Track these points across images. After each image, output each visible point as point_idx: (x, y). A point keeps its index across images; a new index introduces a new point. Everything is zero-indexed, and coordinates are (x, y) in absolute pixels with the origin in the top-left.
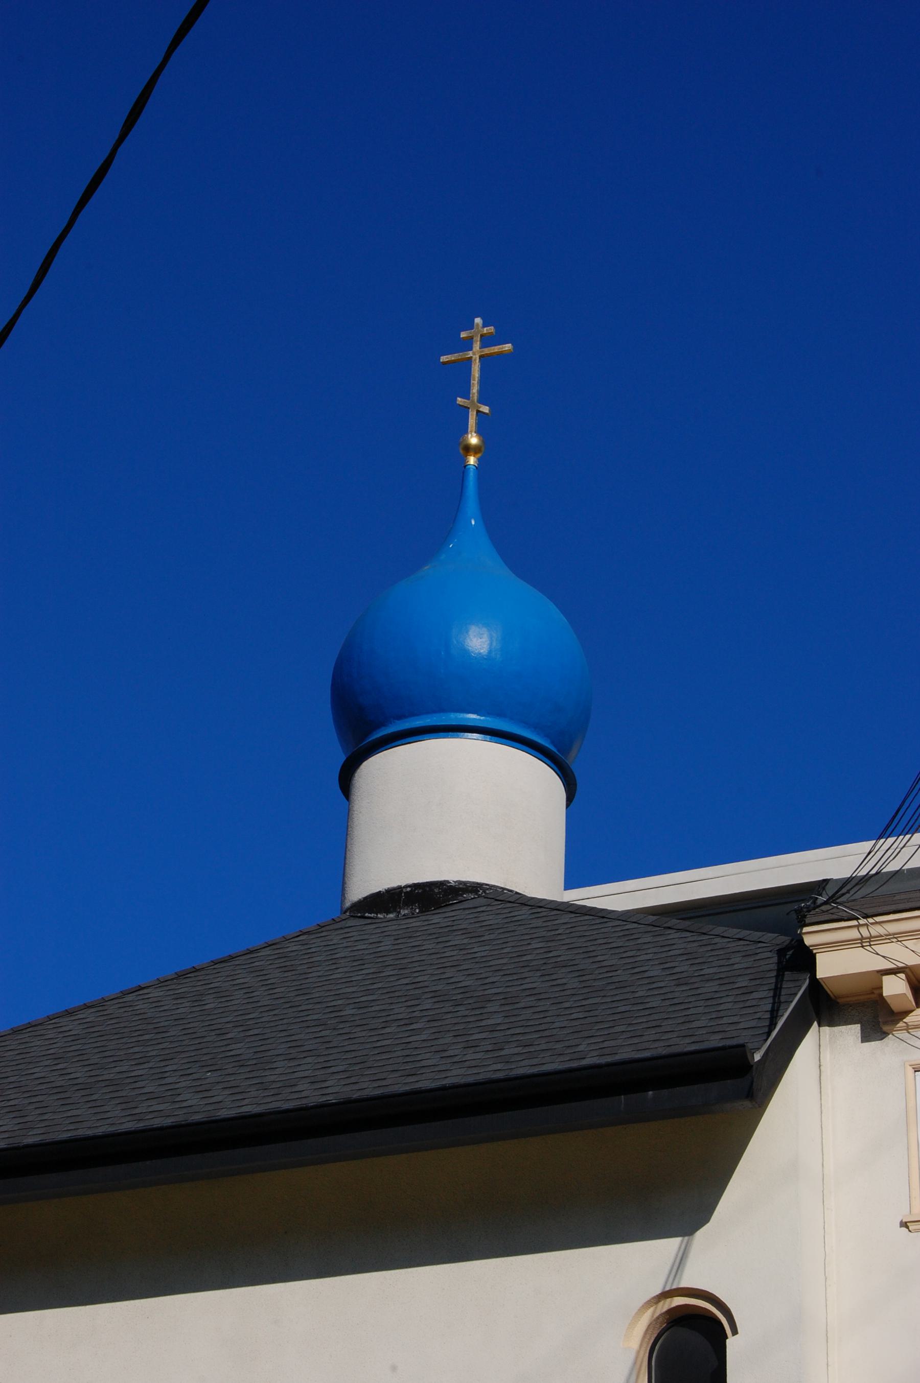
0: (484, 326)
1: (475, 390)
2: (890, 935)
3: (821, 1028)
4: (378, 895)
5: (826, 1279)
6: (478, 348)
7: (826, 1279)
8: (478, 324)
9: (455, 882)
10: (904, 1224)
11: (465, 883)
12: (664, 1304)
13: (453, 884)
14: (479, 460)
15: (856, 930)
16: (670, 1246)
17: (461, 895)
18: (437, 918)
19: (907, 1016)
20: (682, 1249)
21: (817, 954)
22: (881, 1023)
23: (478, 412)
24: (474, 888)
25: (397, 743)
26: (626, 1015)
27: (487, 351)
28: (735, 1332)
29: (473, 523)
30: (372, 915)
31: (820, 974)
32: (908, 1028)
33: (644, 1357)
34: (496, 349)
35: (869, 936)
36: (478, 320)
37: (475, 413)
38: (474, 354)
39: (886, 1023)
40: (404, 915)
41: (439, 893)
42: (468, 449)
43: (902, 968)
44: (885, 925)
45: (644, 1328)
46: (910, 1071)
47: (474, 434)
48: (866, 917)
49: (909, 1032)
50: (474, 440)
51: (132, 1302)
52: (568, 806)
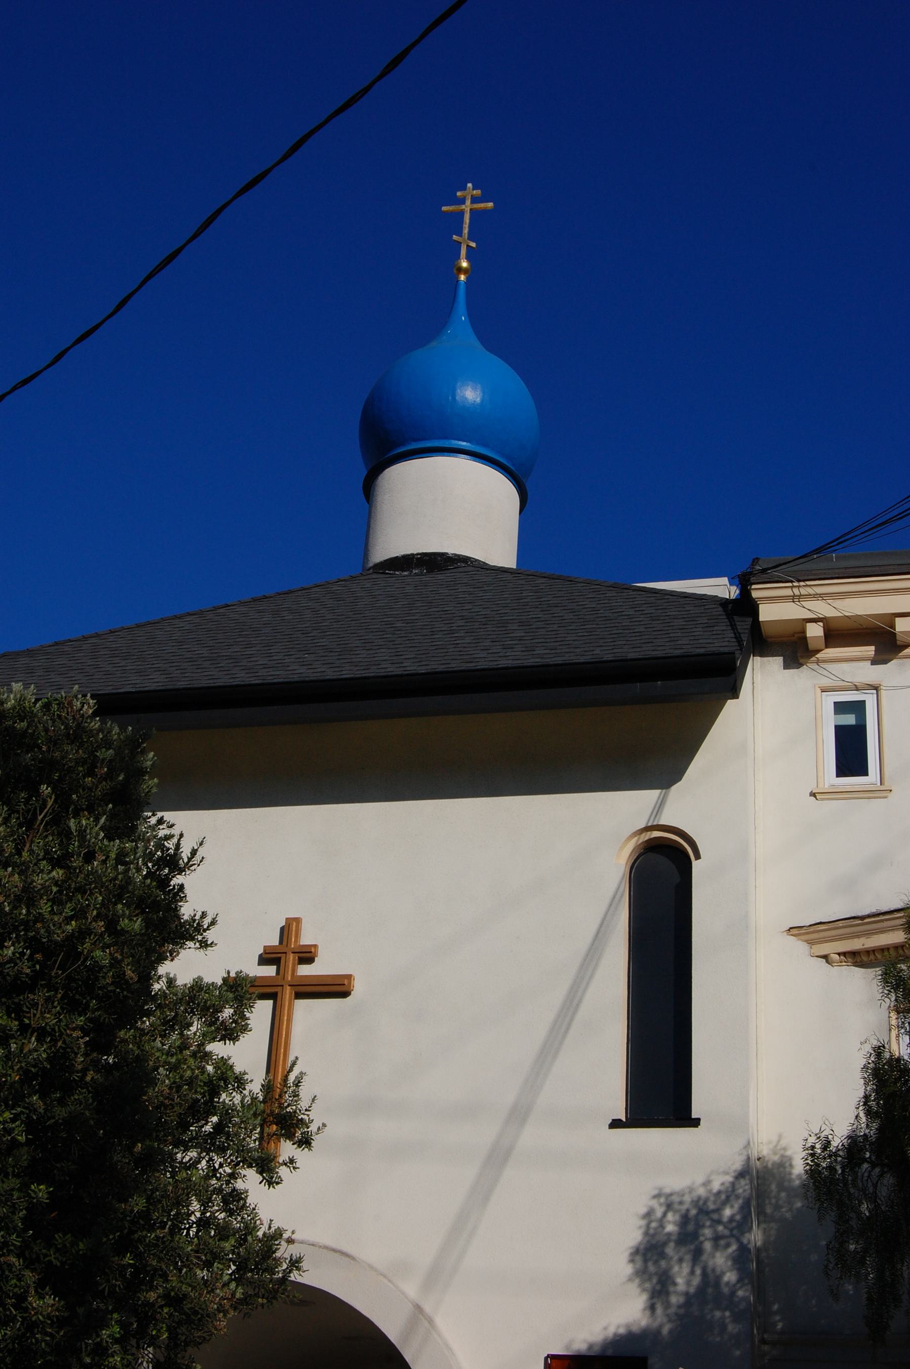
0: (473, 189)
1: (466, 231)
2: (811, 595)
3: (755, 658)
4: (396, 558)
5: (755, 828)
6: (469, 203)
7: (755, 828)
8: (469, 188)
10: (813, 794)
11: (459, 556)
12: (645, 835)
13: (451, 555)
14: (467, 278)
15: (790, 590)
16: (651, 796)
17: (457, 564)
18: (441, 576)
19: (818, 653)
20: (661, 799)
21: (760, 605)
22: (799, 658)
23: (468, 246)
24: (465, 560)
25: (414, 457)
26: (620, 635)
27: (476, 206)
28: (698, 857)
29: (463, 318)
30: (391, 572)
31: (762, 618)
35: (793, 594)
37: (465, 247)
38: (466, 207)
39: (802, 657)
40: (415, 573)
41: (441, 561)
42: (460, 270)
43: (822, 618)
44: (814, 588)
45: (630, 852)
46: (819, 691)
48: (799, 581)
49: (818, 665)
50: (465, 264)
51: (244, 809)
52: (520, 514)
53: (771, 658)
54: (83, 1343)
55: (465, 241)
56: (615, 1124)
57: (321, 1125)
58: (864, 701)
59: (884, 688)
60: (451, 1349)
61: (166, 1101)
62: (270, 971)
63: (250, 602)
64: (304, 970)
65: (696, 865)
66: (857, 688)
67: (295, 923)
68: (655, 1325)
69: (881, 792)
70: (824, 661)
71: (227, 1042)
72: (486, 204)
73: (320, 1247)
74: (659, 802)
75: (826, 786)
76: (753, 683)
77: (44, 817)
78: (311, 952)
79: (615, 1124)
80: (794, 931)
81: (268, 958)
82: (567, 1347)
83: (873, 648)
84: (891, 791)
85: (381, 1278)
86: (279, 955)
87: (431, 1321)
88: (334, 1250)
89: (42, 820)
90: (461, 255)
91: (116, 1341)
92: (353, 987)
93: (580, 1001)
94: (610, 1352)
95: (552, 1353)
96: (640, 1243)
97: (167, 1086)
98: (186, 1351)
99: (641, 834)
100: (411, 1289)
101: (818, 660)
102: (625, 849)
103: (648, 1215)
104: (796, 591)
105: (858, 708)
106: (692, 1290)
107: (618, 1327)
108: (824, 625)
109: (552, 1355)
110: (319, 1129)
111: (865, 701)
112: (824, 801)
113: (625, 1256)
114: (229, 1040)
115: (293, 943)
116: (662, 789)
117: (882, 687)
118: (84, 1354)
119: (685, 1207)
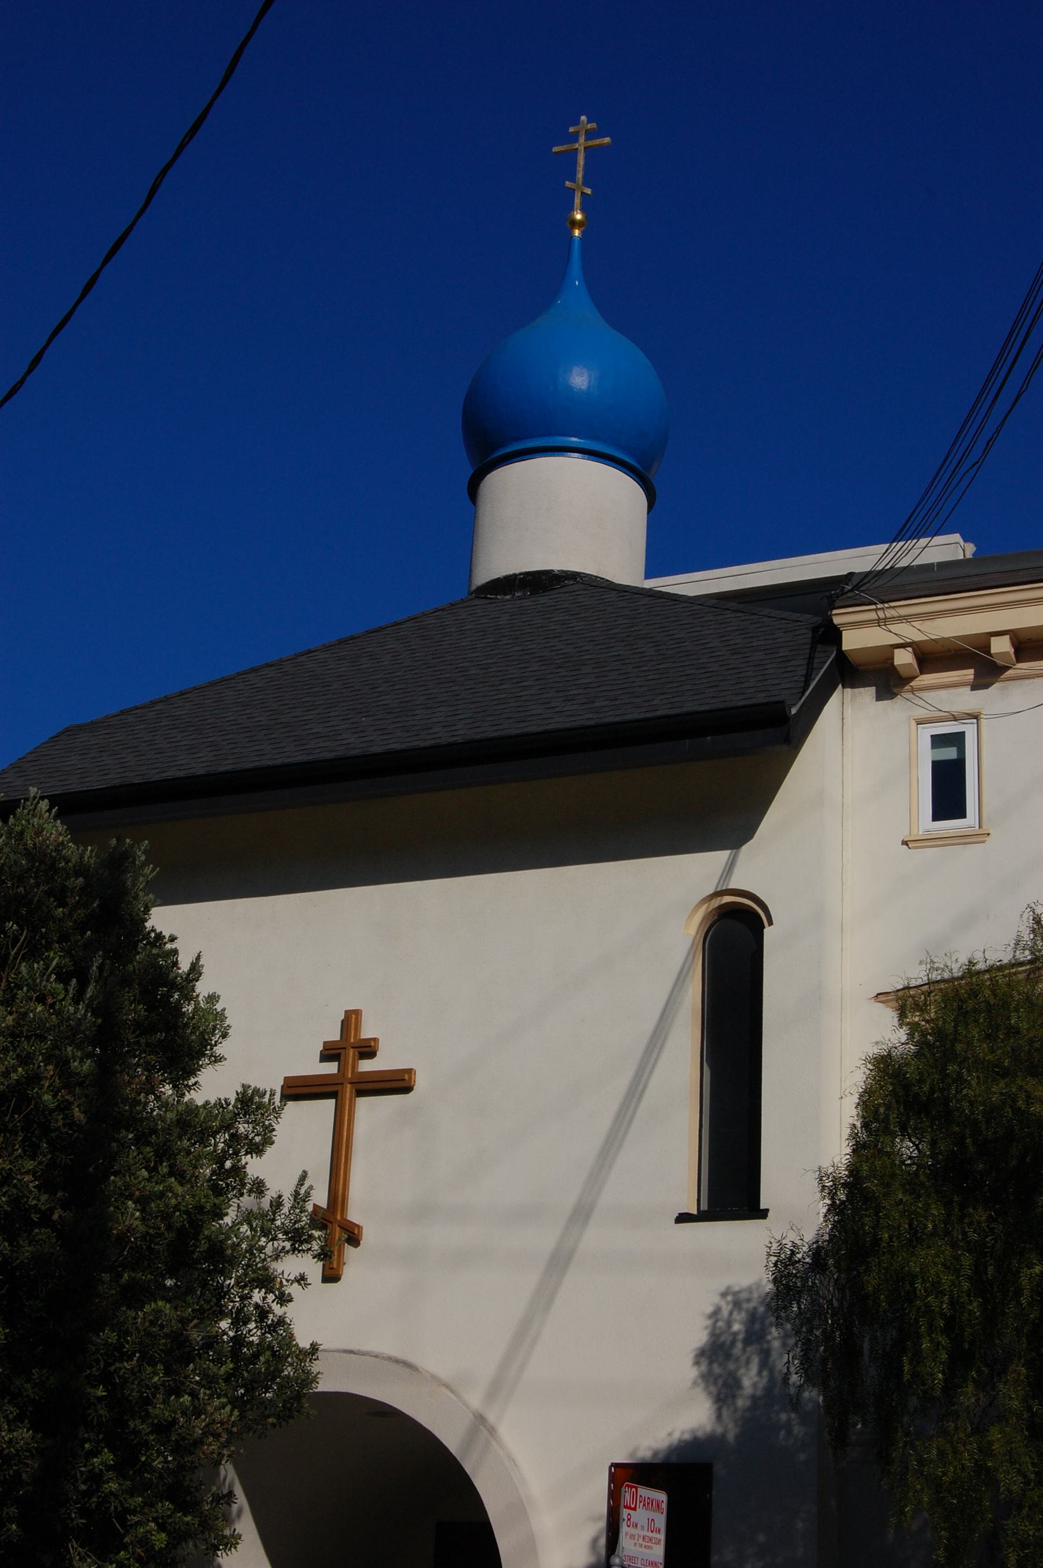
1: (580, 175)
6: (583, 140)
8: (583, 121)
9: (559, 571)
10: (905, 843)
13: (557, 573)
14: (583, 233)
16: (719, 858)
20: (731, 860)
23: (582, 193)
24: (574, 576)
25: (516, 460)
28: (771, 923)
29: (577, 283)
30: (493, 596)
34: (597, 142)
36: (583, 118)
37: (580, 194)
38: (580, 145)
39: (896, 686)
42: (574, 224)
43: (910, 643)
44: (898, 610)
46: (914, 723)
47: (579, 212)
48: (883, 602)
51: (303, 894)
52: (648, 514)
53: (863, 689)
54: (78, 1471)
55: (580, 188)
56: (683, 1218)
58: (964, 733)
59: (984, 717)
60: (513, 1460)
61: (151, 1231)
62: (331, 1068)
63: (336, 645)
64: (366, 1066)
65: (768, 932)
66: (955, 719)
67: (354, 1016)
68: (719, 1430)
69: (979, 836)
70: (921, 689)
71: (254, 1155)
73: (384, 1358)
74: (729, 863)
75: (921, 833)
76: (843, 719)
77: (20, 950)
78: (371, 1046)
79: (683, 1218)
80: (882, 998)
81: (329, 1054)
82: (632, 1455)
83: (972, 671)
84: (989, 834)
85: (443, 1389)
86: (337, 1051)
87: (492, 1431)
88: (397, 1361)
89: (17, 954)
91: (109, 1468)
92: (415, 1081)
94: (674, 1459)
95: (617, 1462)
96: (705, 1345)
97: (138, 1218)
98: (194, 1473)
99: (711, 900)
100: (475, 1400)
102: (695, 918)
103: (715, 1314)
104: (881, 614)
105: (957, 740)
106: (759, 1393)
107: (683, 1433)
108: (913, 650)
109: (616, 1464)
111: (964, 732)
112: (917, 850)
113: (689, 1358)
114: (256, 1153)
115: (352, 1037)
117: (982, 716)
118: (80, 1482)
119: (752, 1305)
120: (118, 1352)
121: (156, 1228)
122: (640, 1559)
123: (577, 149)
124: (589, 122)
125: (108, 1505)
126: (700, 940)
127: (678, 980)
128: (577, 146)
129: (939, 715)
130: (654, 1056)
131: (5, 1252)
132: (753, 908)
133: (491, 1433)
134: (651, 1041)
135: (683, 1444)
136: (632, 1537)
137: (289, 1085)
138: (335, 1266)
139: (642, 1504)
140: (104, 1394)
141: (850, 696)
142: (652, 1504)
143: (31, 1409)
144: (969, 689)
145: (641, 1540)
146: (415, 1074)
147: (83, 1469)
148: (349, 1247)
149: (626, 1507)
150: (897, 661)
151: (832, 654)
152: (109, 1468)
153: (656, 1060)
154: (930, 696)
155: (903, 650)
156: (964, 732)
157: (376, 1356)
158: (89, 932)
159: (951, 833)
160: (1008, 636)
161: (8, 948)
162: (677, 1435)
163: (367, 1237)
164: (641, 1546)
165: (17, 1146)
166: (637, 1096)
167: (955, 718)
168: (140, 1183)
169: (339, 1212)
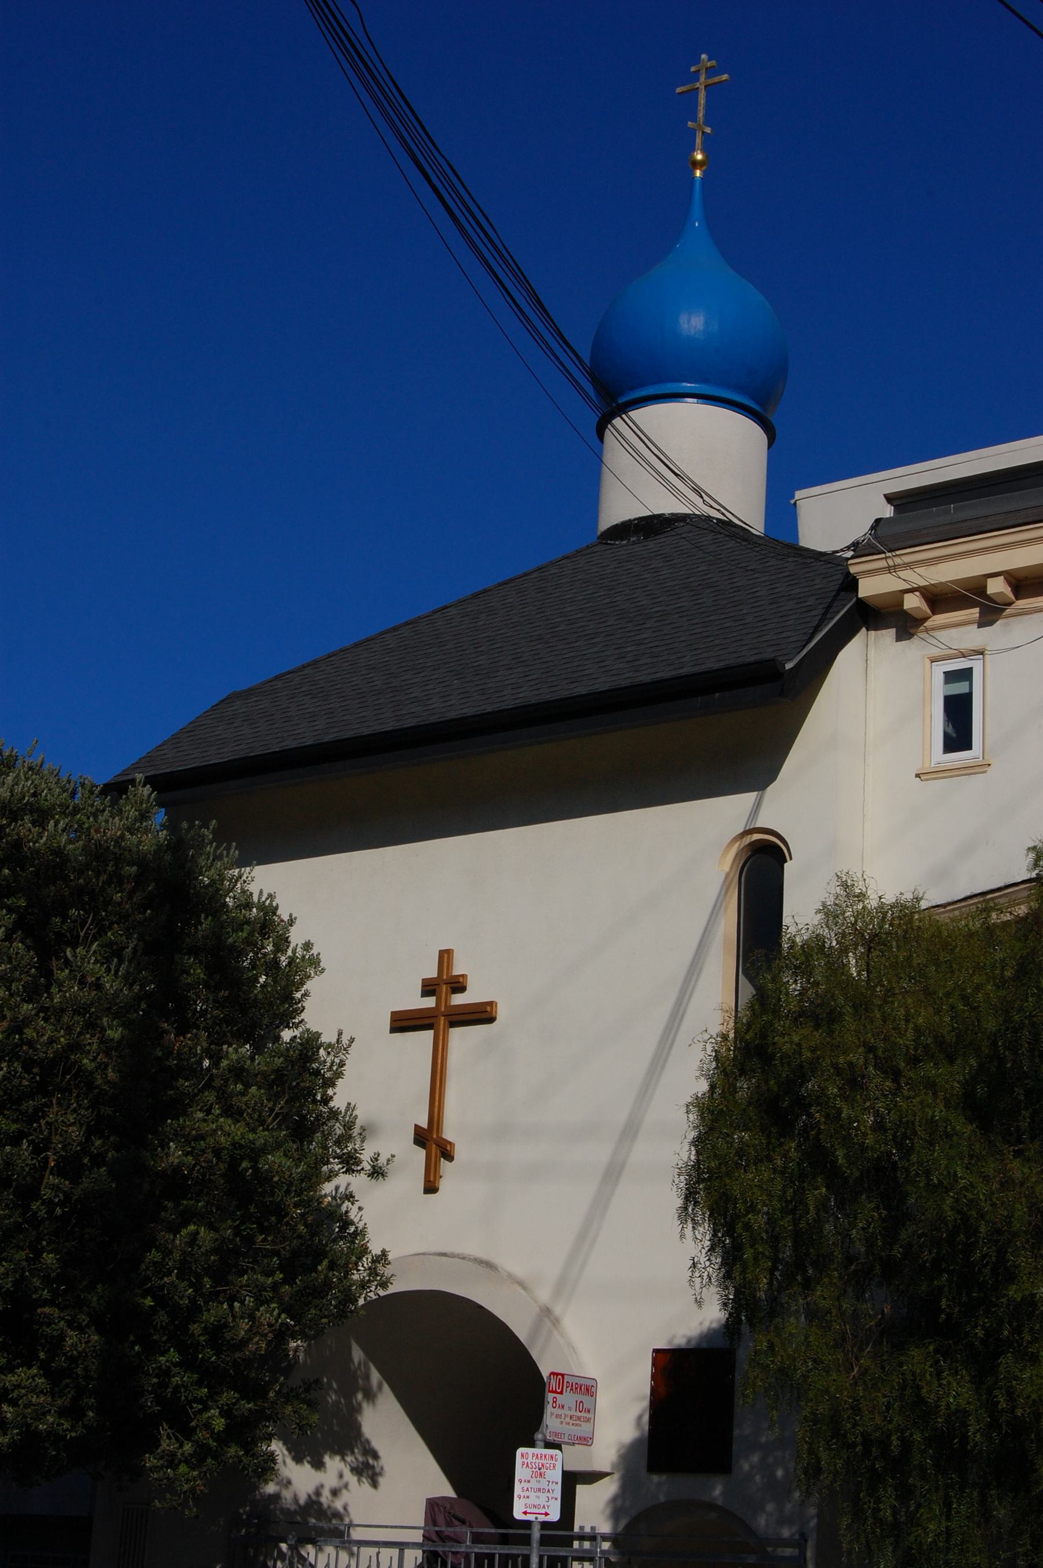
1: (701, 115)
3: (869, 632)
6: (703, 79)
8: (703, 60)
9: (669, 514)
10: (918, 776)
13: (668, 516)
14: (704, 173)
15: (884, 561)
16: (751, 797)
17: (674, 524)
21: (860, 580)
23: (703, 132)
28: (791, 859)
29: (697, 225)
32: (927, 631)
33: (734, 877)
34: (716, 79)
36: (704, 56)
39: (911, 627)
42: (695, 164)
46: (928, 661)
47: (699, 152)
48: (890, 551)
50: (699, 157)
51: (407, 845)
52: (769, 448)
55: (701, 127)
57: (390, 1157)
58: (971, 668)
59: (989, 653)
60: (573, 1348)
62: (430, 1002)
64: (458, 999)
69: (980, 768)
70: (933, 629)
72: (719, 77)
73: (470, 1260)
74: (756, 804)
76: (867, 660)
78: (459, 982)
81: (429, 988)
82: (670, 1342)
84: (989, 765)
87: (556, 1322)
90: (697, 145)
92: (496, 1013)
93: (685, 1011)
94: (704, 1345)
100: (544, 1295)
101: (926, 629)
105: (966, 675)
107: (711, 1322)
109: (657, 1349)
110: (388, 1160)
111: (972, 668)
116: (758, 790)
117: (986, 652)
120: (160, 1269)
121: (208, 1162)
122: (566, 1436)
123: (698, 88)
124: (709, 60)
125: (179, 1395)
126: (735, 875)
127: (712, 913)
128: (698, 85)
129: (951, 653)
130: (692, 983)
131: (66, 1189)
132: (776, 844)
133: (554, 1324)
134: (689, 971)
135: (712, 1332)
136: (557, 1416)
137: (395, 1019)
138: (432, 1179)
139: (569, 1389)
140: (152, 1304)
141: (873, 638)
142: (581, 1389)
143: (109, 1316)
144: (976, 626)
145: (568, 1420)
146: (496, 1006)
147: (154, 1366)
148: (446, 1161)
149: (552, 1392)
150: (907, 606)
151: (850, 602)
152: (176, 1365)
153: (694, 987)
154: (942, 635)
155: (911, 594)
156: (972, 668)
157: (464, 1258)
158: (149, 911)
159: (957, 765)
160: (1002, 577)
161: (78, 931)
162: (706, 1325)
163: (459, 1152)
164: (568, 1424)
165: (73, 1101)
166: (678, 1020)
167: (963, 655)
168: (195, 1124)
169: (435, 1131)
